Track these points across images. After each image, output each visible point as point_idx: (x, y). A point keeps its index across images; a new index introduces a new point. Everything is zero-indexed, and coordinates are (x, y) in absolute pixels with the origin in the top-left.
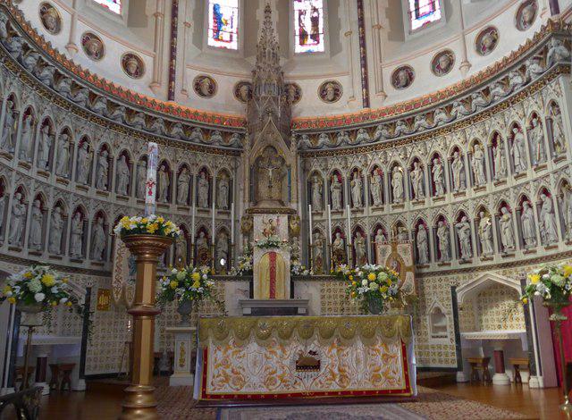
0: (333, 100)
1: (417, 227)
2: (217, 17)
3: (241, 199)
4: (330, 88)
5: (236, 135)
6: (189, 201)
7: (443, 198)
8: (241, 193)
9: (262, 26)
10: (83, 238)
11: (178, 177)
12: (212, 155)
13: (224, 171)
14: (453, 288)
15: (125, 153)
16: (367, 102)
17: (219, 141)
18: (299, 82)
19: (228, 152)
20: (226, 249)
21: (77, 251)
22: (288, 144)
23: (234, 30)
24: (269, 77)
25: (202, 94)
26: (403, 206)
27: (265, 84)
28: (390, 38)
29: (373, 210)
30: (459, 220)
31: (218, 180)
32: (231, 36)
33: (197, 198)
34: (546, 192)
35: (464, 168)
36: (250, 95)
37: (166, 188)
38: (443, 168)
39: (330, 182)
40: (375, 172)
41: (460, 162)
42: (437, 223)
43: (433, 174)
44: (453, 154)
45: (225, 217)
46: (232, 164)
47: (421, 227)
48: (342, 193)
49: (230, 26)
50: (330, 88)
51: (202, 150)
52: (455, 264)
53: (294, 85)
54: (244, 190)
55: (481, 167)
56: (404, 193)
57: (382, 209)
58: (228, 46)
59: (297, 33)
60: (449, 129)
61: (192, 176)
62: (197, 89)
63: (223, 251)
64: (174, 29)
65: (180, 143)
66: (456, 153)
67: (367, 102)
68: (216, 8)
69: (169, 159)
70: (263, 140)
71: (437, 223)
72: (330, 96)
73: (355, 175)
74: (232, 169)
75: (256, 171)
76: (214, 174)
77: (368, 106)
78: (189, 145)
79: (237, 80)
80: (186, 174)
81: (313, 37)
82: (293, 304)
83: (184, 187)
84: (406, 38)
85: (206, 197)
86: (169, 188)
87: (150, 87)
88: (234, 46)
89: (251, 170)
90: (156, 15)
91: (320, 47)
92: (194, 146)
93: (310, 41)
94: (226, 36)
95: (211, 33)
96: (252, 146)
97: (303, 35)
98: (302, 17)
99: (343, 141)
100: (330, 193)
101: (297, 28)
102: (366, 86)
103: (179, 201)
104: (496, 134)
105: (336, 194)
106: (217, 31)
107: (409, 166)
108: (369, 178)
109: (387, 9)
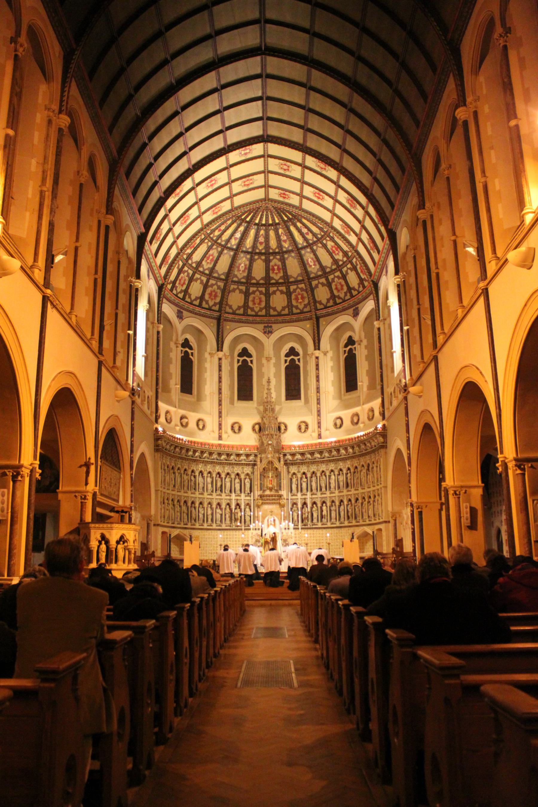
1: (340, 503)
3: (256, 489)
10: (188, 515)
13: (248, 474)
15: (201, 472)
17: (245, 460)
19: (249, 465)
21: (186, 520)
25: (235, 432)
30: (356, 502)
31: (245, 479)
33: (245, 520)
34: (350, 500)
36: (260, 430)
39: (301, 478)
45: (248, 498)
47: (342, 503)
48: (307, 484)
76: (243, 476)
83: (228, 485)
85: (239, 488)
86: (221, 486)
89: (261, 475)
96: (261, 461)
100: (301, 485)
104: (369, 464)
105: (304, 485)
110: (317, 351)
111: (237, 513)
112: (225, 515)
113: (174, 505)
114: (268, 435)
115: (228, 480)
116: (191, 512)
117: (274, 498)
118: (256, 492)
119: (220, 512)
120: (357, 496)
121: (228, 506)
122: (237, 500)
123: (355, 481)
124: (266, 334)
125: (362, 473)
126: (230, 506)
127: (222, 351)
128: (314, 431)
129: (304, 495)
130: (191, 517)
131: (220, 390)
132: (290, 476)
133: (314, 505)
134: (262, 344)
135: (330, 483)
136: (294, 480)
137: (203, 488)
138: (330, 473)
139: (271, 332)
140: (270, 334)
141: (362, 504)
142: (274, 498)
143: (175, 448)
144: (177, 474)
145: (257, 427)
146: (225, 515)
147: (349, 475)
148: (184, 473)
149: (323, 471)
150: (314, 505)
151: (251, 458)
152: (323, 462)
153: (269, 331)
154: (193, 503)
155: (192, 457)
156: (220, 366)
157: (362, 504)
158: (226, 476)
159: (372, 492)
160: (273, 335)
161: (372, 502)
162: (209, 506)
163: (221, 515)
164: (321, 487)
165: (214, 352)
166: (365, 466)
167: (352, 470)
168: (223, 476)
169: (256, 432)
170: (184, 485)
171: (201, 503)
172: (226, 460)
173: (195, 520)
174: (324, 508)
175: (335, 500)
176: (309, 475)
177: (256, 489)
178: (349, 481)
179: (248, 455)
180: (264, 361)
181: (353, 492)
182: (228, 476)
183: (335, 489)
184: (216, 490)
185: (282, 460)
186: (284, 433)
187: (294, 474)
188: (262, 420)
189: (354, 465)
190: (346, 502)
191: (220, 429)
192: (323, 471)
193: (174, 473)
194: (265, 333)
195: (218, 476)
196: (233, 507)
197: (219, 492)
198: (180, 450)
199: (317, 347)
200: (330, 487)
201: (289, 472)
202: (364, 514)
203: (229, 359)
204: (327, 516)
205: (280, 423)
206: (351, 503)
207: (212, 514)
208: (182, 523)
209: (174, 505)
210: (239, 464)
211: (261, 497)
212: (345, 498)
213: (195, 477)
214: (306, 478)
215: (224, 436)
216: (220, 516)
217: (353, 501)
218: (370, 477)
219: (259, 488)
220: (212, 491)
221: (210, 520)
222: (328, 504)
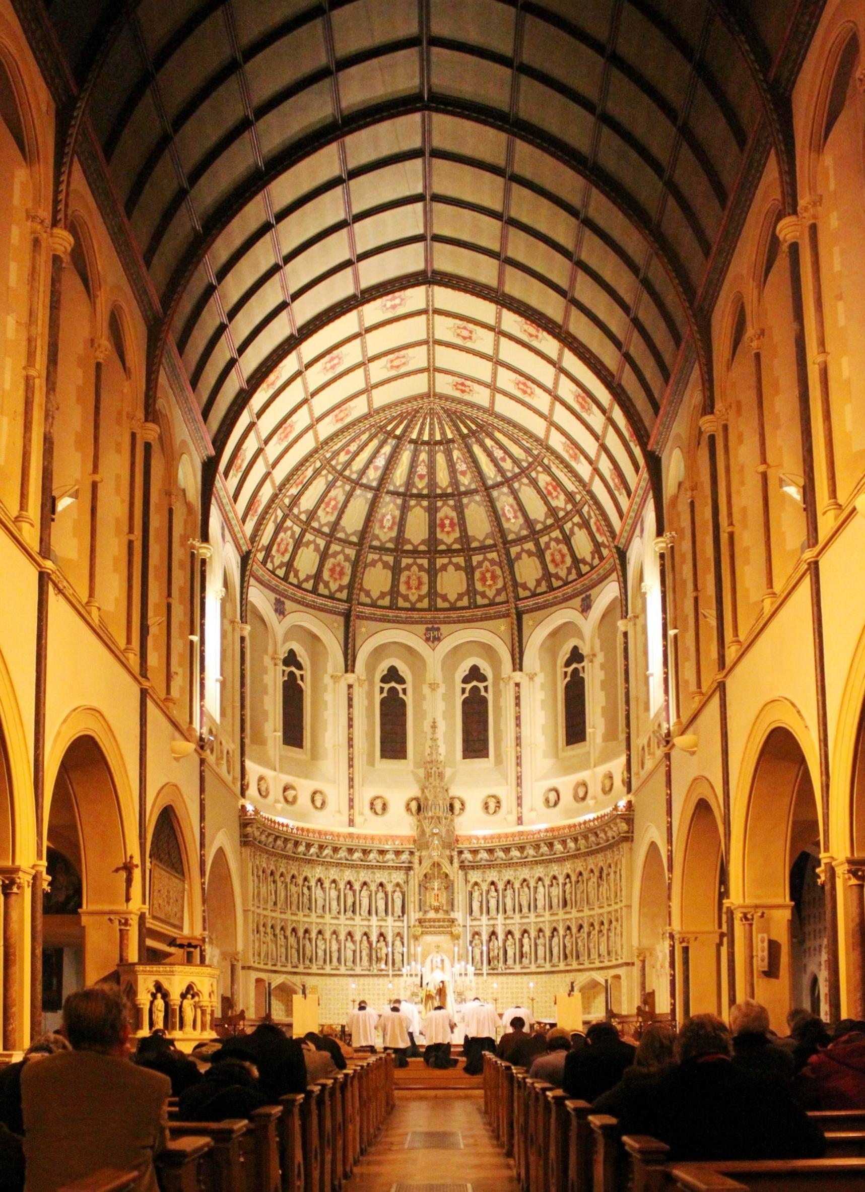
1: (553, 933)
7: (570, 913)
10: (298, 951)
13: (398, 885)
14: (572, 983)
21: (295, 960)
30: (579, 931)
33: (393, 960)
34: (569, 928)
36: (419, 809)
39: (488, 892)
45: (399, 924)
46: (404, 877)
47: (555, 933)
48: (498, 901)
52: (575, 965)
69: (352, 880)
75: (424, 886)
76: (389, 888)
83: (365, 902)
86: (354, 903)
89: (420, 885)
96: (420, 863)
100: (488, 902)
104: (602, 869)
107: (549, 883)
111: (381, 949)
112: (361, 952)
113: (275, 935)
114: (432, 818)
115: (365, 893)
116: (304, 946)
117: (441, 923)
119: (353, 947)
120: (580, 922)
121: (365, 937)
122: (381, 927)
123: (578, 896)
124: (430, 643)
125: (590, 884)
126: (368, 938)
127: (353, 672)
130: (304, 955)
132: (469, 888)
133: (510, 937)
135: (536, 900)
136: (476, 894)
139: (438, 639)
140: (436, 643)
141: (589, 934)
142: (441, 923)
144: (279, 884)
145: (414, 805)
146: (361, 952)
147: (568, 886)
148: (291, 882)
153: (434, 637)
154: (306, 931)
155: (305, 855)
157: (589, 934)
158: (362, 888)
161: (605, 932)
162: (334, 936)
163: (354, 952)
164: (520, 906)
165: (339, 674)
166: (595, 871)
167: (574, 878)
168: (357, 887)
171: (320, 932)
172: (362, 861)
173: (311, 961)
174: (526, 941)
175: (543, 928)
176: (501, 887)
178: (568, 897)
179: (398, 852)
180: (426, 690)
181: (574, 914)
182: (365, 887)
183: (545, 909)
184: (345, 911)
187: (476, 884)
189: (578, 870)
190: (561, 932)
192: (525, 880)
193: (274, 882)
195: (348, 886)
196: (374, 938)
199: (518, 666)
201: (467, 881)
202: (592, 951)
205: (452, 798)
206: (571, 932)
207: (339, 951)
208: (289, 965)
209: (275, 935)
210: (384, 868)
213: (309, 888)
214: (496, 890)
215: (358, 819)
216: (351, 953)
218: (603, 889)
220: (339, 913)
221: (335, 960)
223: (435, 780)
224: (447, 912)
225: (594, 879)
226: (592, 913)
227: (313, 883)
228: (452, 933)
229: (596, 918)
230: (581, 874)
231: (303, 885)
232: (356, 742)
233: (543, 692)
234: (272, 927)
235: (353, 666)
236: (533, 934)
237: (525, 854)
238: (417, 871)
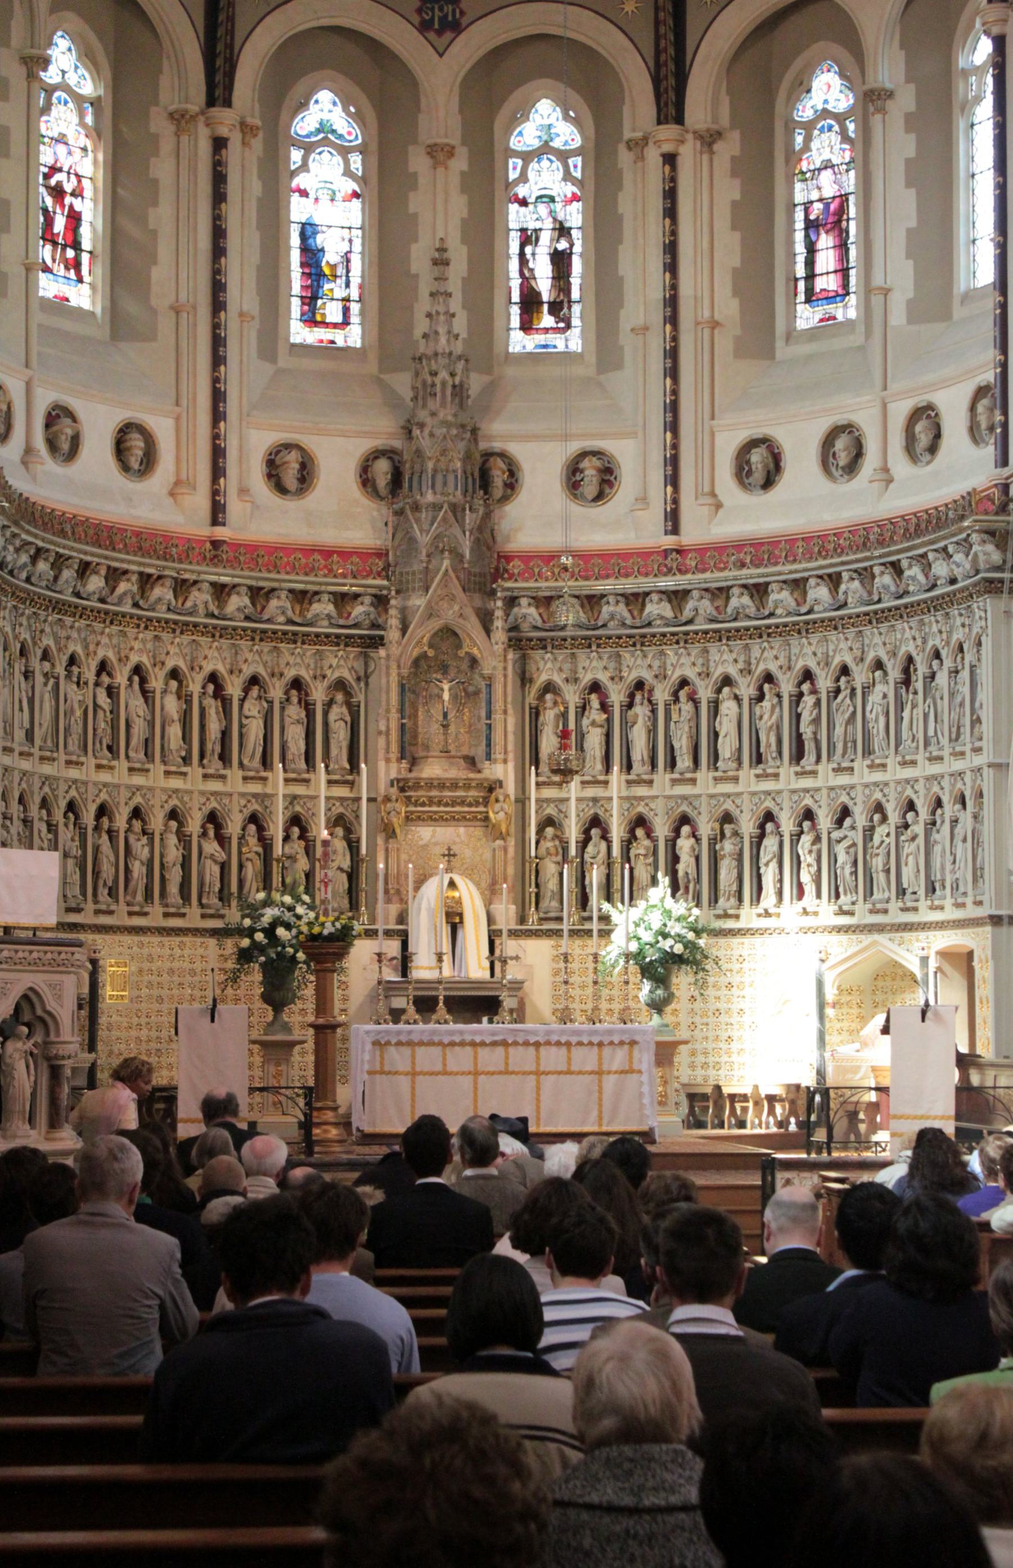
0: (600, 497)
1: (762, 827)
2: (311, 255)
3: (381, 754)
4: (590, 468)
5: (367, 600)
6: (266, 762)
7: (814, 773)
8: (382, 741)
9: (424, 289)
11: (241, 707)
12: (310, 650)
13: (340, 685)
16: (673, 521)
17: (329, 617)
18: (515, 449)
20: (346, 864)
22: (486, 620)
23: (355, 294)
24: (444, 452)
25: (281, 489)
26: (736, 779)
27: (435, 471)
28: (741, 351)
29: (674, 782)
30: (839, 823)
31: (329, 704)
32: (346, 311)
34: (809, 815)
35: (854, 713)
37: (219, 736)
38: (818, 703)
39: (583, 708)
40: (682, 694)
41: (848, 701)
42: (800, 825)
43: (799, 716)
44: (838, 680)
46: (359, 665)
47: (769, 827)
49: (341, 281)
50: (590, 468)
51: (293, 638)
53: (503, 455)
54: (388, 733)
55: (882, 720)
56: (740, 749)
57: (693, 781)
58: (339, 338)
59: (516, 297)
60: (833, 624)
61: (270, 703)
62: (270, 476)
63: (340, 869)
64: (218, 342)
65: (244, 629)
66: (843, 679)
67: (673, 521)
68: (308, 231)
70: (431, 613)
71: (800, 825)
72: (590, 488)
73: (638, 698)
74: (359, 679)
76: (318, 694)
77: (675, 530)
78: (264, 631)
79: (366, 445)
80: (260, 697)
81: (555, 308)
82: (492, 989)
83: (255, 729)
84: (779, 354)
87: (172, 494)
88: (353, 336)
89: (402, 687)
90: (176, 310)
91: (574, 341)
92: (275, 632)
93: (547, 320)
94: (333, 312)
95: (296, 306)
96: (404, 630)
97: (530, 302)
98: (528, 250)
99: (612, 617)
101: (515, 284)
102: (673, 480)
103: (246, 762)
104: (910, 660)
106: (311, 299)
107: (752, 691)
108: (667, 705)
109: (735, 272)
110: (669, 131)
111: (292, 858)
112: (241, 867)
113: (26, 822)
114: (436, 507)
115: (253, 708)
116: (97, 849)
117: (460, 793)
118: (382, 765)
119: (222, 856)
120: (844, 799)
121: (252, 828)
122: (294, 798)
123: (839, 731)
124: (431, 35)
125: (875, 698)
126: (261, 829)
127: (228, 103)
128: (643, 500)
129: (639, 782)
130: (96, 874)
131: (218, 287)
132: (531, 699)
133: (640, 832)
134: (412, 83)
135: (715, 735)
136: (549, 716)
137: (148, 743)
138: (719, 691)
139: (455, 27)
140: (448, 35)
141: (869, 832)
142: (460, 793)
143: (34, 559)
144: (39, 679)
145: (382, 468)
146: (241, 867)
147: (809, 700)
148: (69, 676)
149: (684, 682)
150: (640, 832)
151: (359, 611)
152: (683, 640)
153: (443, 19)
154: (102, 811)
155: (102, 600)
156: (219, 179)
157: (869, 832)
158: (246, 691)
159: (920, 786)
160: (463, 36)
161: (919, 829)
162: (174, 824)
163: (224, 867)
164: (671, 750)
165: (194, 108)
166: (889, 665)
167: (824, 683)
168: (234, 689)
169: (382, 499)
170: (67, 730)
171: (136, 813)
172: (247, 618)
173: (112, 892)
174: (685, 845)
175: (735, 812)
176: (617, 696)
177: (381, 754)
178: (806, 730)
179: (344, 596)
180: (418, 162)
181: (826, 776)
182: (255, 691)
183: (739, 760)
184: (202, 756)
185: (498, 623)
186: (505, 499)
187: (549, 687)
188: (408, 432)
189: (836, 661)
190: (787, 824)
191: (218, 472)
192: (684, 682)
193: (27, 674)
194: (424, 27)
195: (211, 688)
196: (276, 829)
197: (215, 765)
198: (53, 566)
199: (672, 111)
200: (715, 756)
201: (524, 679)
202: (880, 878)
203: (257, 144)
204: (698, 880)
205: (488, 455)
206: (814, 826)
207: (185, 864)
208: (123, 908)
209: (26, 822)
210: (307, 639)
211: (402, 790)
212: (786, 805)
213: (111, 692)
214: (604, 707)
215: (235, 507)
216: (216, 869)
217: (825, 821)
218: (912, 715)
219: (394, 747)
220: (186, 760)
221: (173, 889)
222: (706, 828)
223: (443, 404)
224: (471, 762)
225: (883, 690)
226: (908, 773)
227: (121, 677)
228: (487, 819)
229: (892, 792)
230: (845, 670)
231: (97, 684)
232: (233, 295)
233: (737, 183)
234: (21, 800)
235: (229, 88)
236: (706, 828)
237: (687, 613)
238: (395, 650)
